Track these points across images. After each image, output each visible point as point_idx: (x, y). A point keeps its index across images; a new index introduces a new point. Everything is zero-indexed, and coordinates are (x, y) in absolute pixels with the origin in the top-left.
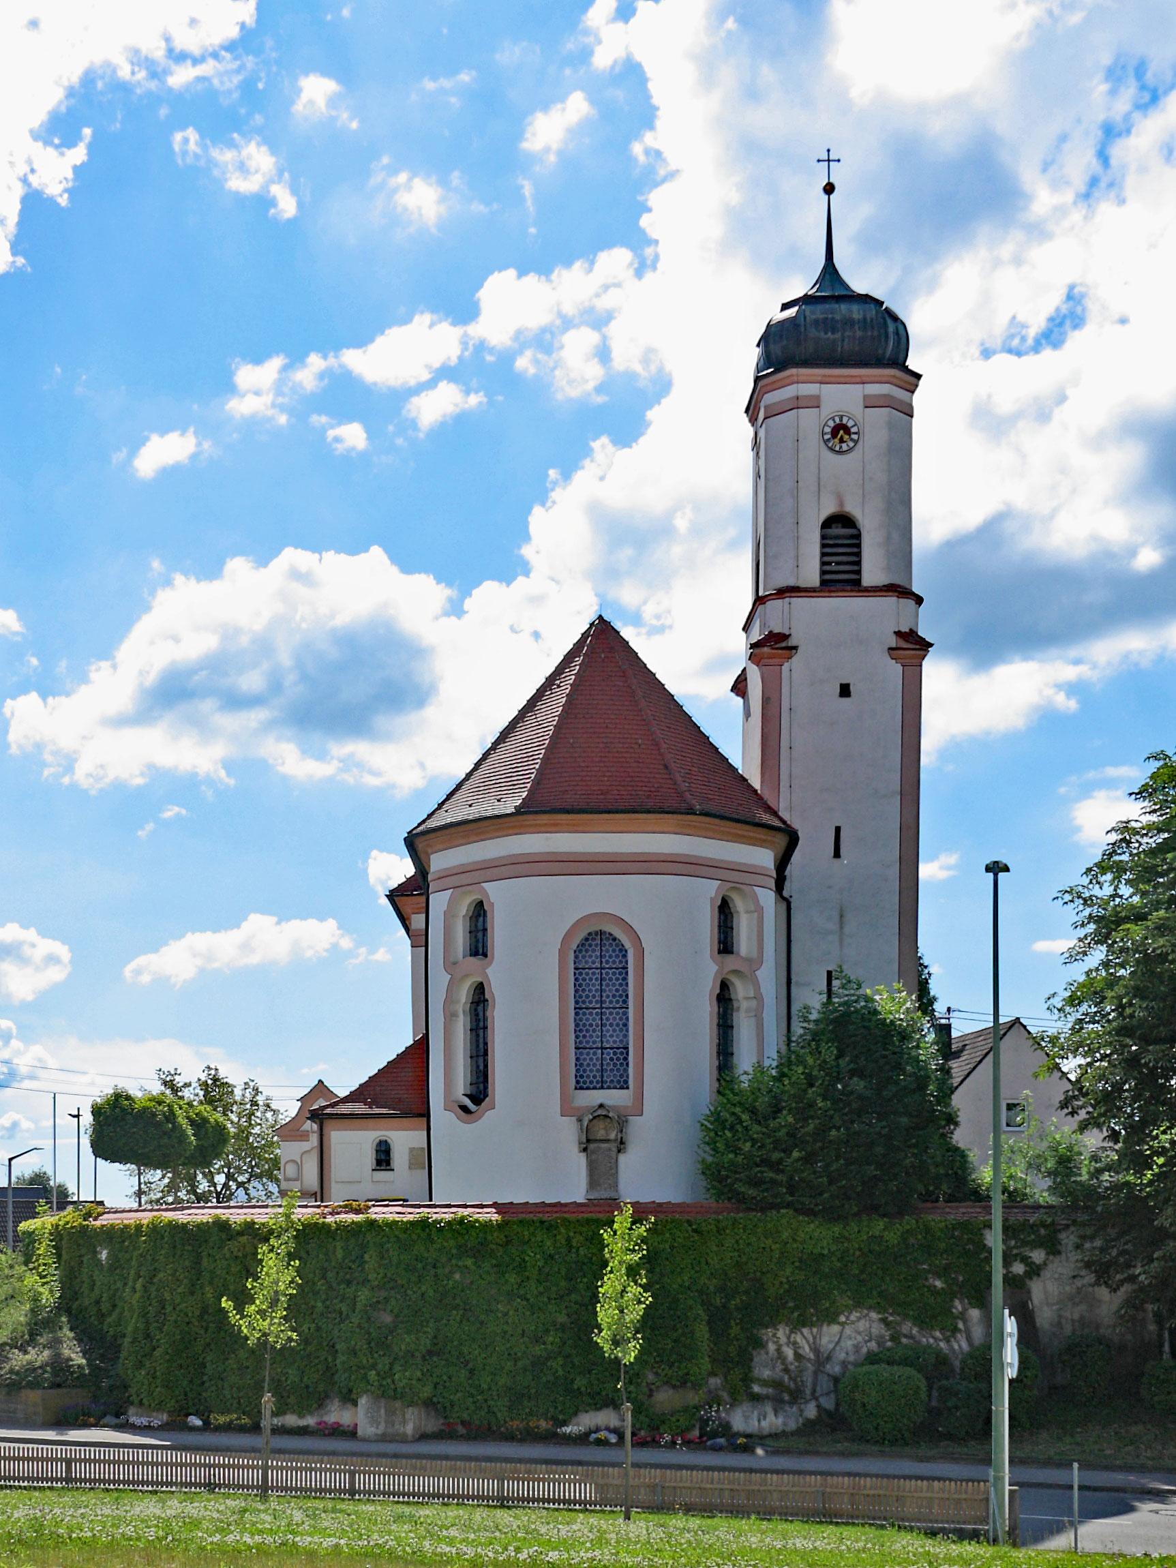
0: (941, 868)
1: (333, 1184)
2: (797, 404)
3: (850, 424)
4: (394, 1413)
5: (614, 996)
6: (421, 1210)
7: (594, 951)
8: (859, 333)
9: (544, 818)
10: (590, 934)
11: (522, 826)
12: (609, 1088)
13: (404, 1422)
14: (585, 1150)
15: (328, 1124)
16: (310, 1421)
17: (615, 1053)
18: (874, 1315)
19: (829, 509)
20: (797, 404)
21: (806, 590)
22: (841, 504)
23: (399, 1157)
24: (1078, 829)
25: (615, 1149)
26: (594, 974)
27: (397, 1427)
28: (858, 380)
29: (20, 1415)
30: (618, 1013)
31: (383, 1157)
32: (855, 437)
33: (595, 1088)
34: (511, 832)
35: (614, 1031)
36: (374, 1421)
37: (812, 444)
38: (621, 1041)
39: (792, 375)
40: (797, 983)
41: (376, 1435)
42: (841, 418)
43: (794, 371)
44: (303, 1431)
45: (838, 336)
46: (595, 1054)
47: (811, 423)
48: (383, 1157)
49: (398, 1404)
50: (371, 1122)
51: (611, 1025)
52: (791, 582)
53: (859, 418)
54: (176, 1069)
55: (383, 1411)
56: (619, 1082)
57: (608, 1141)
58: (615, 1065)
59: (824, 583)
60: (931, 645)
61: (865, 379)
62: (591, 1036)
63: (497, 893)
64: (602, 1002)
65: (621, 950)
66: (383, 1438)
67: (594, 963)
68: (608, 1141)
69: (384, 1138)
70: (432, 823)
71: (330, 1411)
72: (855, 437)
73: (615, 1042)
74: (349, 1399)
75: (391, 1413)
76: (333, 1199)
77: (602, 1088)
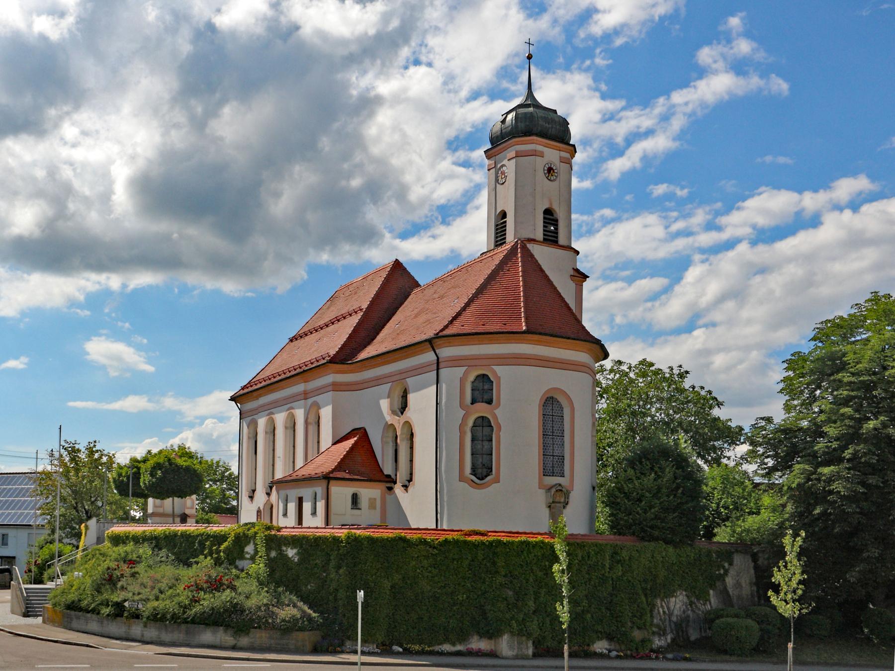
0: (21, 363)
1: (332, 515)
2: (534, 153)
3: (554, 168)
4: (522, 643)
5: (558, 430)
6: (397, 531)
7: (549, 406)
8: (558, 127)
9: (536, 337)
10: (548, 398)
11: (524, 340)
12: (556, 476)
13: (527, 648)
14: (549, 507)
15: (332, 482)
16: (459, 648)
17: (558, 459)
18: (684, 593)
19: (546, 206)
20: (534, 153)
21: (537, 241)
22: (551, 204)
23: (364, 502)
24: (88, 354)
25: (562, 507)
26: (549, 418)
27: (524, 650)
28: (558, 148)
29: (292, 647)
30: (560, 439)
31: (355, 499)
32: (556, 174)
33: (550, 476)
34: (513, 341)
35: (558, 447)
36: (511, 647)
37: (541, 175)
38: (561, 453)
39: (533, 140)
40: (237, 417)
41: (513, 655)
42: (551, 164)
43: (535, 138)
44: (459, 654)
45: (550, 126)
46: (550, 458)
47: (540, 164)
48: (355, 499)
49: (524, 638)
50: (348, 482)
51: (557, 444)
52: (532, 237)
53: (558, 165)
54: (76, 441)
55: (516, 642)
56: (560, 473)
57: (560, 502)
58: (558, 465)
59: (544, 239)
60: (588, 277)
61: (561, 149)
62: (548, 449)
63: (502, 372)
64: (553, 432)
65: (561, 408)
66: (516, 657)
67: (549, 412)
68: (560, 502)
69: (355, 492)
70: (441, 334)
71: (471, 642)
72: (556, 174)
73: (558, 453)
74: (492, 634)
75: (519, 643)
76: (332, 523)
77: (553, 476)
